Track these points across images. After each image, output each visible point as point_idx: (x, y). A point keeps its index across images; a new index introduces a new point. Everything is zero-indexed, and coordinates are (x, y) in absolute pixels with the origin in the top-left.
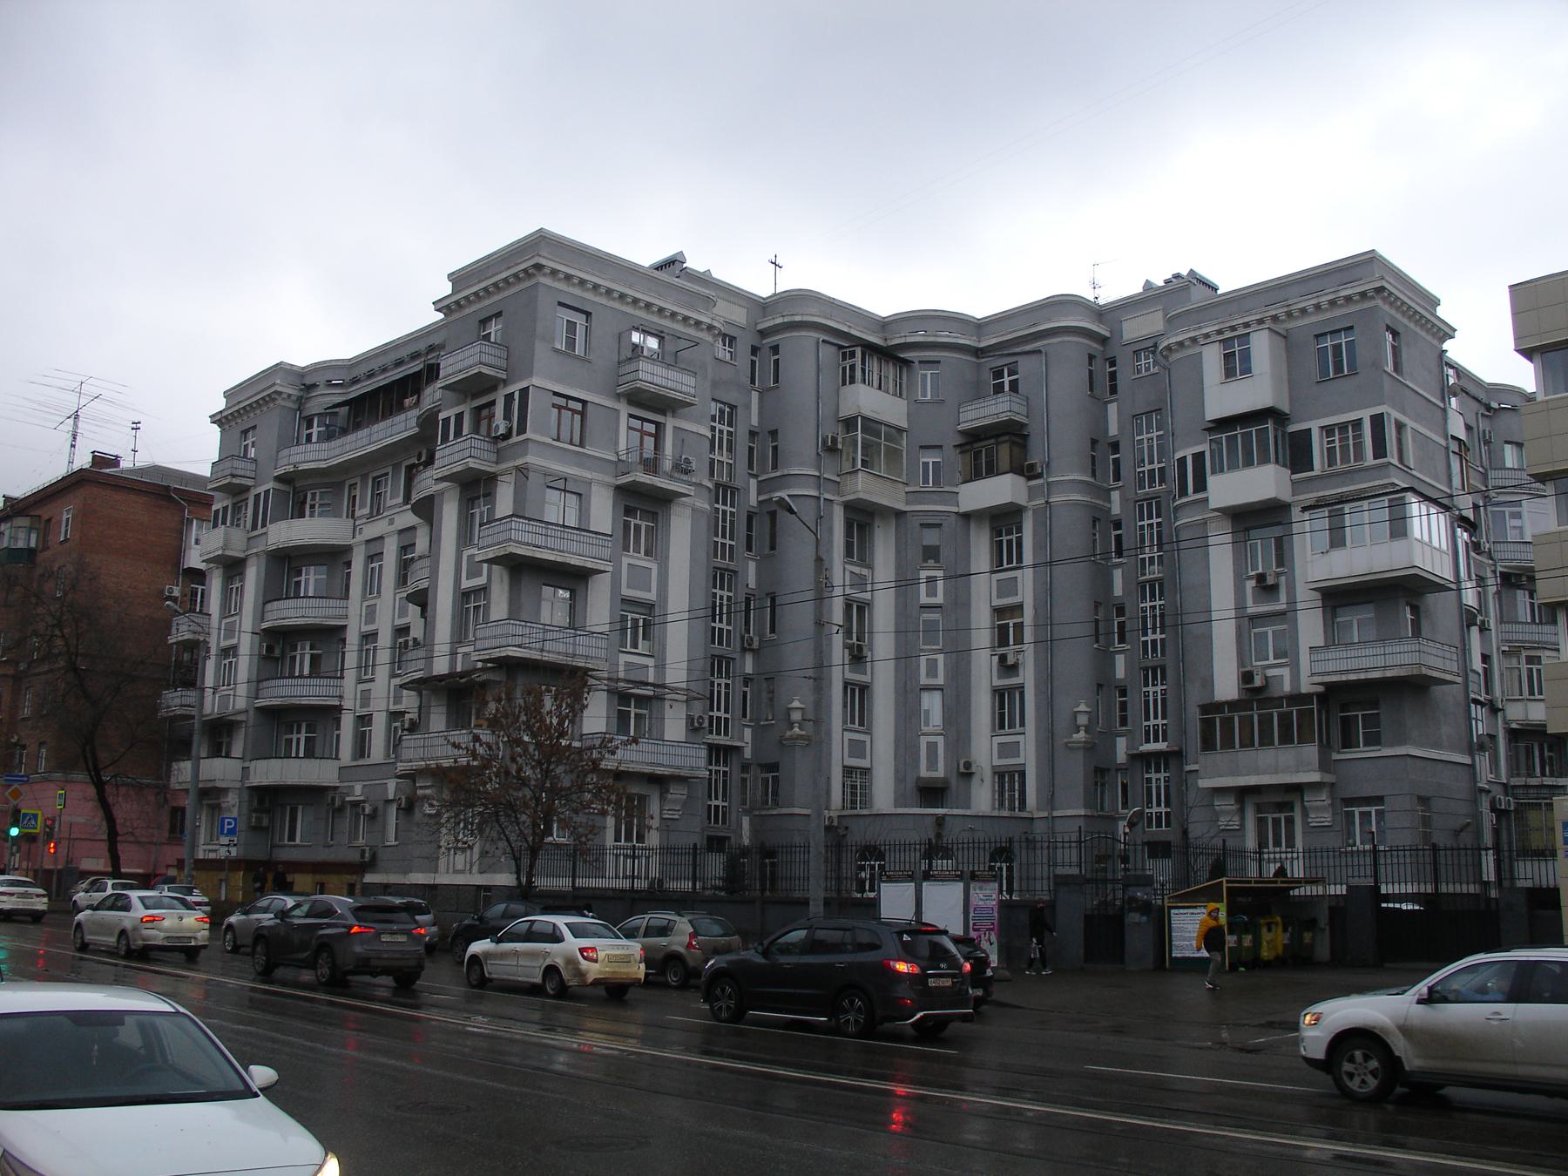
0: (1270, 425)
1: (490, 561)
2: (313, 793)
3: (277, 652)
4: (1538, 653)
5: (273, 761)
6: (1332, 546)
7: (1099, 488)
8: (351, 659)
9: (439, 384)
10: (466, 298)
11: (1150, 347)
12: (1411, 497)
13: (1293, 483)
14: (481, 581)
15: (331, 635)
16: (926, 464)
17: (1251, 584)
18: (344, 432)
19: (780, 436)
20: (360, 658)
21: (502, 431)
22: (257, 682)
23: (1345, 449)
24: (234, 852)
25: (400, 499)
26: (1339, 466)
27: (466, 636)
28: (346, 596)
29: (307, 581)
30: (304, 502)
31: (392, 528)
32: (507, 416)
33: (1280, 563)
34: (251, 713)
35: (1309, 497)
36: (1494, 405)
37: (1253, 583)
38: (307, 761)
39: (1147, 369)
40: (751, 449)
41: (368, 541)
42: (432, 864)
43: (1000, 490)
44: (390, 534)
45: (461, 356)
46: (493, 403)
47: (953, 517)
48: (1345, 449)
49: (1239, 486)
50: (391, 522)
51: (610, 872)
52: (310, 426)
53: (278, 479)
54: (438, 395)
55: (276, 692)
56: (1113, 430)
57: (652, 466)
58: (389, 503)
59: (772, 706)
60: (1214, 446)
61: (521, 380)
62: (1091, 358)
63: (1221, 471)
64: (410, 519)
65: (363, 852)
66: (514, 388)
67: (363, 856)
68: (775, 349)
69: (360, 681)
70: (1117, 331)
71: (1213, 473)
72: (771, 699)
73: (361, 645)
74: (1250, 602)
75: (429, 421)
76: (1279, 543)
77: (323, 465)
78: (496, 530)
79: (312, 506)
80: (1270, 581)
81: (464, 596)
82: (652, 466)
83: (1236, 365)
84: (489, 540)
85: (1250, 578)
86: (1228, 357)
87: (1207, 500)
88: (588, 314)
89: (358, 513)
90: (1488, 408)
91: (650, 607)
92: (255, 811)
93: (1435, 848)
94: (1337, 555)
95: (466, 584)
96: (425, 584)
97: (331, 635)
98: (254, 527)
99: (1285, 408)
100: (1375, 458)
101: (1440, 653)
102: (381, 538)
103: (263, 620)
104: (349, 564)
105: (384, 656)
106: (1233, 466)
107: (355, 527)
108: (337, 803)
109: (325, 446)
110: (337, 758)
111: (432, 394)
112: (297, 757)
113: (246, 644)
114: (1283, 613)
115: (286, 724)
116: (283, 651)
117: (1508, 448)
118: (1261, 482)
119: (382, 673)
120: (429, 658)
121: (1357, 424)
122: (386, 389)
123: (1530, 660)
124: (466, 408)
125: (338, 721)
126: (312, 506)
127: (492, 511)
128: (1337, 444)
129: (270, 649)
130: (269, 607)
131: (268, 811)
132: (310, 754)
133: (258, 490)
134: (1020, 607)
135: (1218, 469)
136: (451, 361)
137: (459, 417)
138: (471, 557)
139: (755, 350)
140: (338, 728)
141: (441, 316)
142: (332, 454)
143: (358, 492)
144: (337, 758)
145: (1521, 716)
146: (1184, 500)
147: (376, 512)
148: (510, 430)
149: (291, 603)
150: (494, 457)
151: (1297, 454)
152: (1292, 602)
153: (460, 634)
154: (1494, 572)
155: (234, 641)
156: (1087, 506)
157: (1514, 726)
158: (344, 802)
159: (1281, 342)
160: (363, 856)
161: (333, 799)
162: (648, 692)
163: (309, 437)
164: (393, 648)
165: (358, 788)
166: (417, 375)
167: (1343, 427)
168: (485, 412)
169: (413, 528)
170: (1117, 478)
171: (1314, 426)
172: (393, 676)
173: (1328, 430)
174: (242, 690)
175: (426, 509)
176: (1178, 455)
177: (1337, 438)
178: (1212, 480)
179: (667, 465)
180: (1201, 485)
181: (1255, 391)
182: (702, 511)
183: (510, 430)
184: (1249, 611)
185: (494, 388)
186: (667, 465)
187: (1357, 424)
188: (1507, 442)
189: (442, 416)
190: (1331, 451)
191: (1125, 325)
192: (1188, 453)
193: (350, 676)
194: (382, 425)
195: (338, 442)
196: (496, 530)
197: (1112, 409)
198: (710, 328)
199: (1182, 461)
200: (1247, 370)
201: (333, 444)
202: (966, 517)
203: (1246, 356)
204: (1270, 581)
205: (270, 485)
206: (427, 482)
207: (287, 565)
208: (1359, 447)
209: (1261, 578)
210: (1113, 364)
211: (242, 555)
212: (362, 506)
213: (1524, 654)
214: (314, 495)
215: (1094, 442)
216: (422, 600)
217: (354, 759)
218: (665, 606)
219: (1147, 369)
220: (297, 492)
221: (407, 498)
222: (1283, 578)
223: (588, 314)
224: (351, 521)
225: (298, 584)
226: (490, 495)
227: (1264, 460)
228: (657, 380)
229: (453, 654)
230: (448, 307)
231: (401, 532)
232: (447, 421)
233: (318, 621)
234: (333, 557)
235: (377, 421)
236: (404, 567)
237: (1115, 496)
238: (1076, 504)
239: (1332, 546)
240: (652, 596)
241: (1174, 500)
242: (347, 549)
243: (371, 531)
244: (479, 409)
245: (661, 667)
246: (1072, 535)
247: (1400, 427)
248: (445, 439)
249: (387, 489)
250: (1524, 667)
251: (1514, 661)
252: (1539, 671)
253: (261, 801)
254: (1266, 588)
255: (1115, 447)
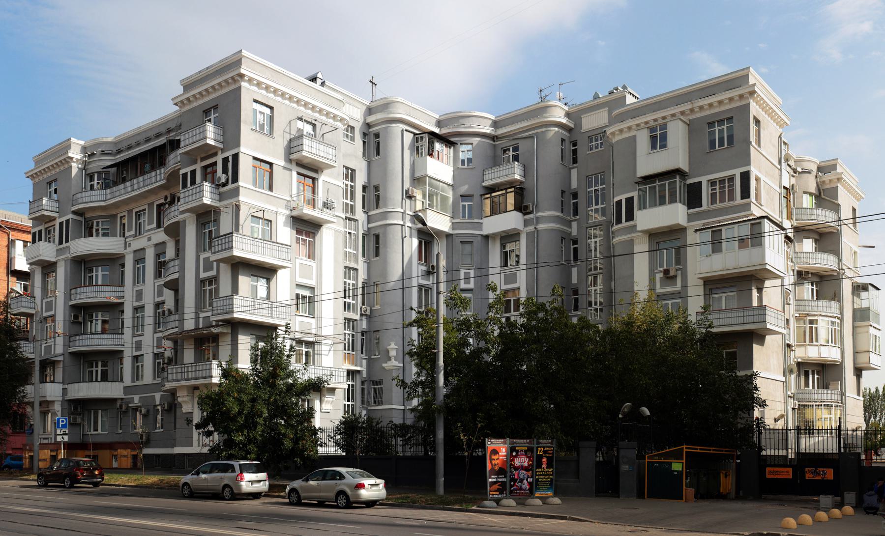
0: (678, 179)
1: (219, 261)
2: (111, 401)
3: (81, 319)
4: (816, 318)
5: (82, 384)
6: (713, 252)
7: (566, 220)
8: (128, 323)
9: (181, 151)
10: (194, 96)
11: (599, 135)
12: (766, 220)
13: (689, 215)
14: (213, 273)
15: (116, 308)
16: (464, 206)
17: (659, 276)
18: (115, 184)
19: (381, 189)
20: (133, 322)
21: (223, 180)
22: (69, 337)
23: (722, 193)
24: (66, 438)
25: (154, 225)
26: (718, 205)
27: (204, 307)
28: (122, 284)
29: (97, 276)
30: (92, 227)
31: (151, 243)
32: (225, 171)
33: (678, 262)
34: (67, 355)
35: (699, 224)
36: (799, 169)
37: (661, 275)
38: (103, 383)
39: (596, 148)
40: (364, 197)
41: (135, 251)
42: (690, 485)
43: (511, 220)
44: (149, 247)
45: (194, 133)
46: (215, 164)
47: (480, 237)
48: (722, 193)
49: (651, 218)
50: (149, 239)
51: (195, 443)
52: (92, 179)
53: (74, 213)
54: (178, 159)
55: (80, 343)
56: (574, 185)
57: (313, 203)
58: (147, 228)
59: (378, 347)
60: (641, 193)
61: (232, 149)
62: (563, 140)
63: (645, 208)
64: (160, 236)
65: (142, 436)
66: (229, 154)
67: (142, 438)
68: (377, 135)
69: (134, 336)
70: (578, 124)
71: (640, 209)
72: (378, 343)
73: (134, 314)
74: (658, 286)
75: (173, 176)
76: (678, 249)
77: (103, 204)
78: (223, 241)
79: (97, 230)
80: (672, 273)
81: (201, 283)
82: (313, 203)
83: (658, 140)
84: (219, 248)
85: (660, 272)
86: (653, 139)
87: (635, 226)
88: (271, 108)
89: (127, 234)
90: (795, 171)
91: (312, 289)
92: (72, 414)
93: (787, 430)
94: (717, 257)
95: (203, 275)
96: (176, 276)
97: (116, 308)
98: (61, 243)
99: (685, 167)
100: (742, 198)
101: (776, 316)
102: (144, 249)
103: (71, 300)
104: (123, 266)
105: (149, 320)
106: (653, 205)
107: (126, 243)
108: (124, 408)
109: (103, 192)
110: (122, 381)
111: (174, 159)
112: (97, 381)
113: (60, 312)
114: (679, 293)
115: (90, 363)
116: (84, 319)
117: (805, 196)
118: (676, 213)
119: (149, 329)
120: (182, 320)
121: (731, 179)
122: (143, 155)
123: (811, 322)
124: (42, 227)
125: (121, 359)
126: (97, 230)
127: (218, 230)
128: (718, 190)
129: (76, 317)
130: (73, 291)
131: (80, 414)
132: (104, 378)
133: (225, 155)
134: (519, 289)
135: (643, 206)
136: (187, 136)
137: (193, 173)
138: (206, 260)
139: (365, 135)
140: (122, 364)
141: (177, 108)
142: (109, 196)
143: (126, 221)
144: (122, 381)
145: (803, 355)
146: (620, 226)
147: (139, 232)
148: (227, 180)
149: (89, 289)
150: (218, 197)
151: (693, 197)
152: (685, 286)
153: (200, 306)
154: (793, 270)
155: (52, 313)
156: (560, 231)
157: (799, 360)
158: (128, 407)
159: (687, 127)
160: (142, 438)
161: (121, 406)
162: (311, 339)
163: (92, 187)
164: (155, 316)
165: (136, 399)
166: (162, 148)
167: (722, 181)
168: (209, 170)
169: (164, 243)
170: (576, 213)
171: (704, 180)
172: (155, 332)
173: (713, 183)
174: (60, 341)
175: (175, 231)
176: (616, 199)
177: (718, 187)
178: (638, 214)
179: (320, 204)
180: (630, 216)
181: (675, 155)
182: (339, 232)
183: (227, 180)
184: (658, 291)
185: (215, 154)
186: (320, 204)
187: (731, 179)
188: (805, 193)
189: (182, 172)
190: (713, 195)
191: (584, 120)
192: (623, 197)
193: (128, 332)
194: (141, 179)
195: (112, 190)
196: (223, 241)
197: (574, 172)
198: (342, 120)
199: (619, 203)
200: (664, 146)
201: (109, 191)
202: (487, 237)
203: (664, 137)
204: (672, 273)
205: (70, 216)
206: (174, 215)
207: (84, 265)
208: (732, 192)
209: (666, 272)
210: (575, 144)
211: (54, 260)
212: (130, 230)
213: (808, 318)
214: (98, 223)
215: (563, 192)
216: (175, 286)
217: (133, 381)
218: (321, 289)
219: (596, 148)
220: (87, 222)
221: (159, 226)
222: (679, 272)
223: (271, 108)
224: (123, 239)
225: (91, 278)
226: (217, 221)
227: (673, 200)
228: (314, 151)
229: (197, 318)
230: (182, 102)
231: (156, 245)
232: (185, 175)
233: (105, 300)
234: (113, 261)
235: (137, 177)
236: (161, 267)
237: (574, 225)
238: (552, 230)
239: (713, 252)
240: (312, 283)
241: (612, 226)
242: (122, 257)
243: (137, 244)
244: (205, 168)
245: (319, 327)
246: (548, 250)
247: (757, 179)
248: (185, 186)
249: (145, 218)
250: (808, 325)
251: (802, 322)
252: (816, 328)
253: (76, 408)
254: (668, 277)
255: (575, 195)
